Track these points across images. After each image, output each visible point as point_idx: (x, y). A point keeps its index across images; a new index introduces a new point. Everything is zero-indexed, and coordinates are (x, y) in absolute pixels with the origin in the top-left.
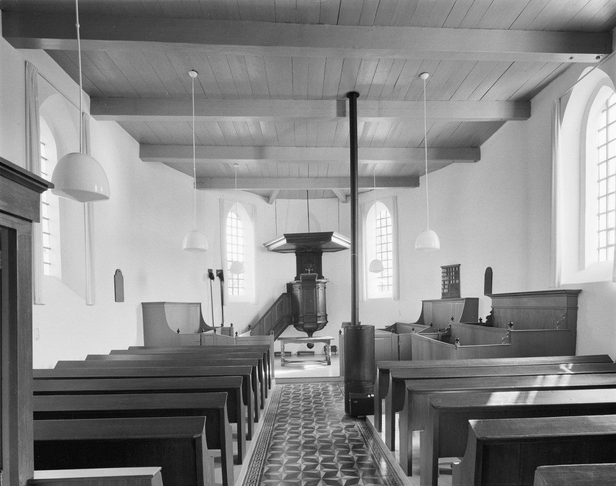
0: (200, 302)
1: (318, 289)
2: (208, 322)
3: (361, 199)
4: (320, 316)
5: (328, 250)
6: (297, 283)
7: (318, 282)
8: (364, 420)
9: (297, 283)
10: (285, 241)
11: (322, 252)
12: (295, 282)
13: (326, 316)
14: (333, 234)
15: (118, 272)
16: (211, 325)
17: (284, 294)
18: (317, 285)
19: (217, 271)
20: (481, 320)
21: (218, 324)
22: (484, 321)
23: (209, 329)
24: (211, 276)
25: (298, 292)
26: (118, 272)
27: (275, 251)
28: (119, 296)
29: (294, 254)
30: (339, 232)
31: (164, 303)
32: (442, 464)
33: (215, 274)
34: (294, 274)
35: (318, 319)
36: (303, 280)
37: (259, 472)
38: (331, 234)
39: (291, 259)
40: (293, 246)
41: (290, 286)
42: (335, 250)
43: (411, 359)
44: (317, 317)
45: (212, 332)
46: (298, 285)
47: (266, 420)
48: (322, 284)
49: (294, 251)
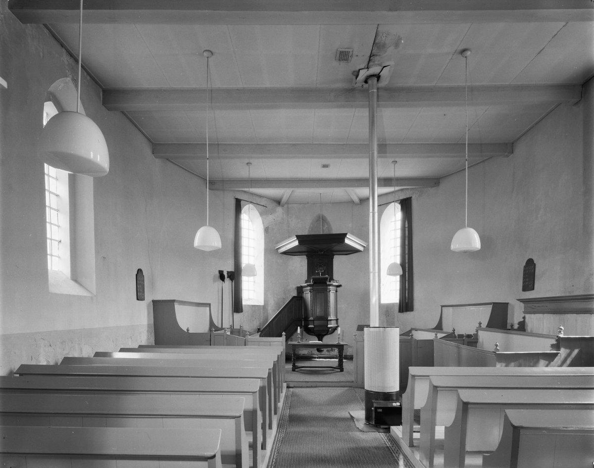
0: (417, 304)
1: (329, 291)
2: (217, 322)
3: (113, 451)
4: (331, 320)
5: (341, 253)
6: (308, 286)
7: (330, 285)
8: (388, 430)
9: (308, 286)
10: (296, 243)
11: (334, 255)
12: (306, 284)
13: (337, 320)
14: (347, 236)
15: (140, 271)
16: (220, 326)
17: (294, 297)
18: (328, 287)
19: (228, 272)
20: (512, 326)
21: (226, 325)
22: (516, 326)
23: (217, 329)
24: (222, 277)
25: (308, 296)
26: (140, 271)
27: (285, 253)
28: (140, 297)
29: (305, 257)
30: (353, 234)
31: (173, 301)
32: (415, 428)
33: (225, 274)
34: (305, 277)
35: (329, 323)
36: (315, 283)
37: (273, 461)
38: (345, 235)
39: (300, 264)
40: (304, 248)
41: (300, 290)
42: (348, 253)
43: (431, 364)
44: (328, 320)
45: (222, 331)
46: (309, 288)
47: (280, 426)
48: (334, 288)
49: (306, 254)
